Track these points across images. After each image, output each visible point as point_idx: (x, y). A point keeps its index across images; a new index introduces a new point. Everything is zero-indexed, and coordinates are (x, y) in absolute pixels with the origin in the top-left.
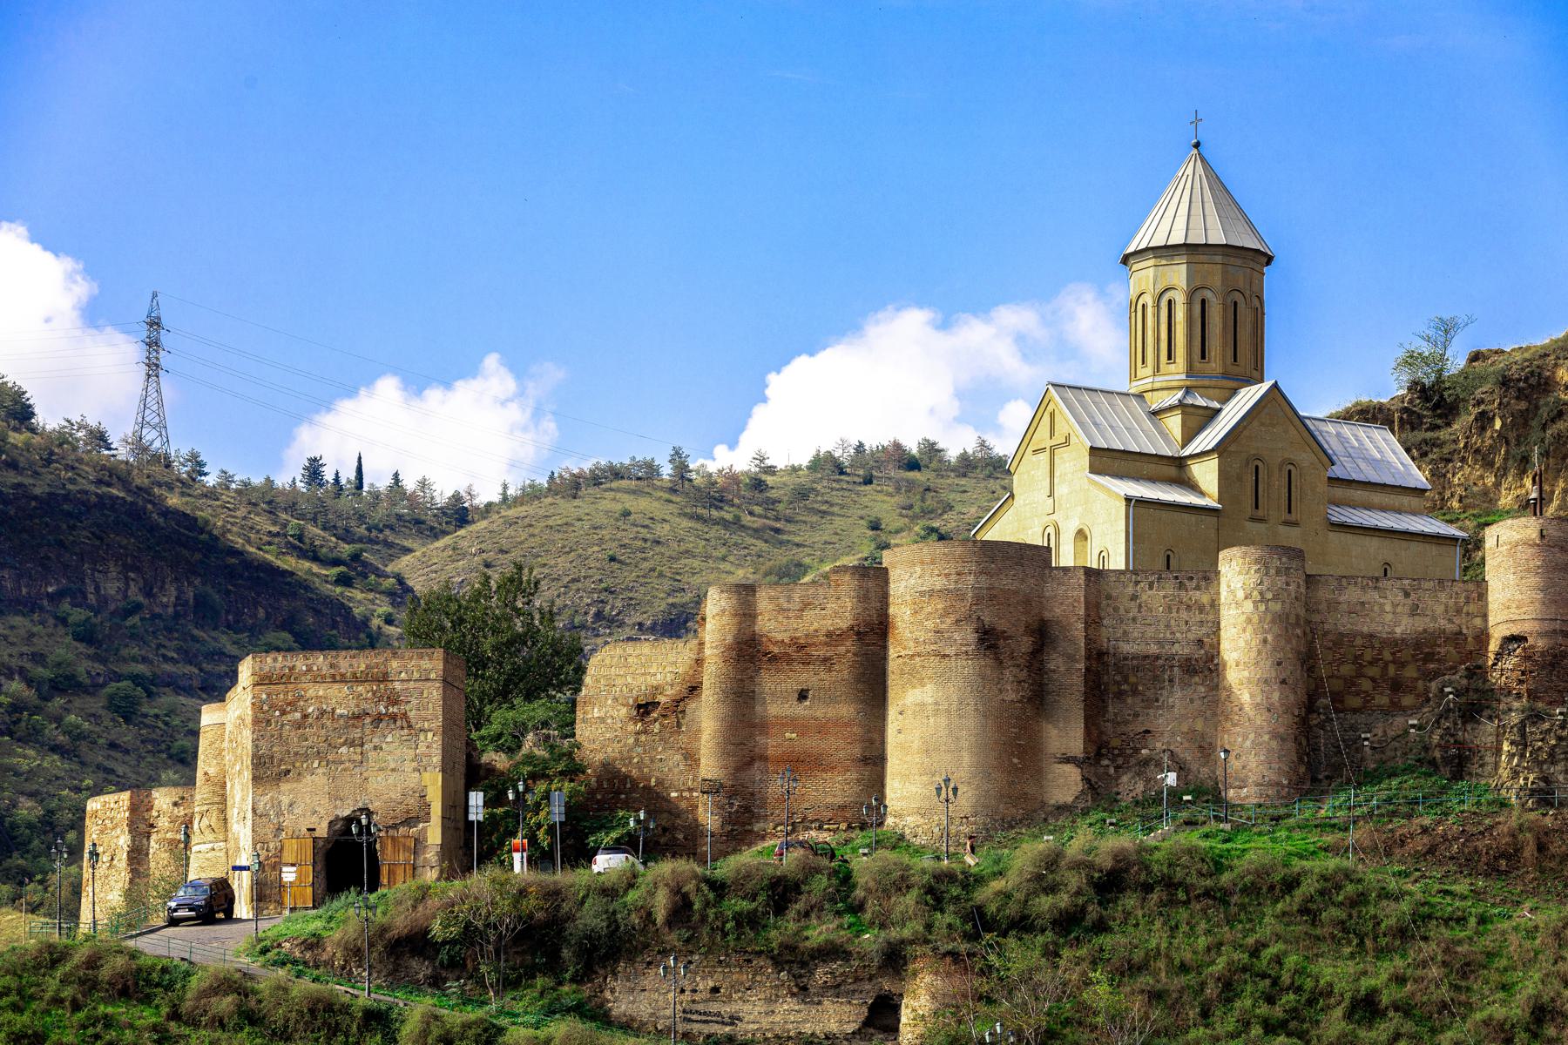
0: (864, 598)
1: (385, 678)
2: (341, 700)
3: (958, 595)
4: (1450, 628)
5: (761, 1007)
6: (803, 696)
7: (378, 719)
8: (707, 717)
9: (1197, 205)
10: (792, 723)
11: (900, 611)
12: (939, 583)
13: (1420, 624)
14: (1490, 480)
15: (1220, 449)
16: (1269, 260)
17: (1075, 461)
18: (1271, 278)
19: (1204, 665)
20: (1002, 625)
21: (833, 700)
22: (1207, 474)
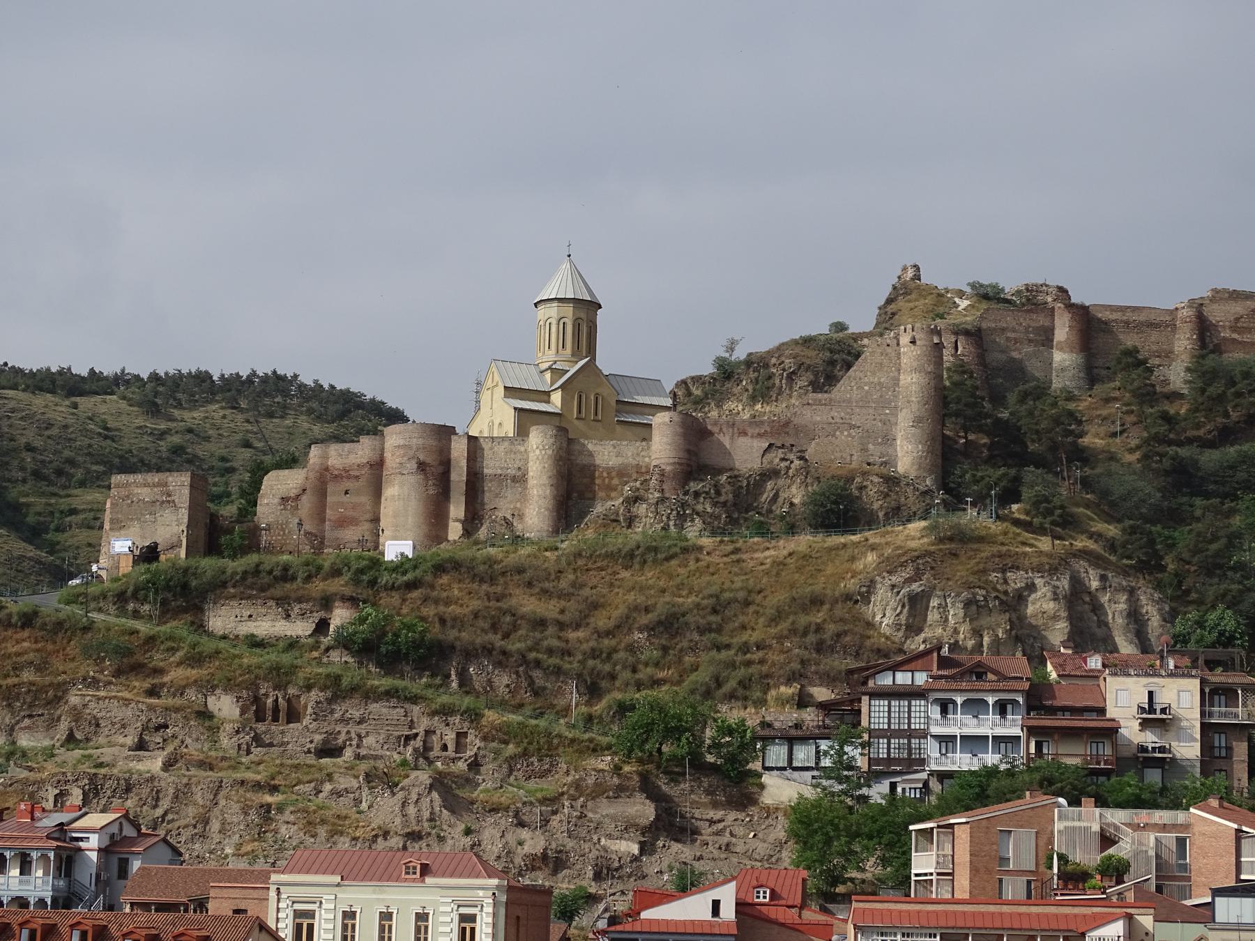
1: (166, 485)
2: (145, 494)
4: (634, 462)
6: (346, 493)
7: (163, 502)
8: (307, 502)
9: (563, 284)
10: (341, 504)
11: (388, 455)
12: (402, 442)
13: (620, 460)
14: (740, 408)
15: (561, 387)
16: (600, 307)
22: (557, 398)
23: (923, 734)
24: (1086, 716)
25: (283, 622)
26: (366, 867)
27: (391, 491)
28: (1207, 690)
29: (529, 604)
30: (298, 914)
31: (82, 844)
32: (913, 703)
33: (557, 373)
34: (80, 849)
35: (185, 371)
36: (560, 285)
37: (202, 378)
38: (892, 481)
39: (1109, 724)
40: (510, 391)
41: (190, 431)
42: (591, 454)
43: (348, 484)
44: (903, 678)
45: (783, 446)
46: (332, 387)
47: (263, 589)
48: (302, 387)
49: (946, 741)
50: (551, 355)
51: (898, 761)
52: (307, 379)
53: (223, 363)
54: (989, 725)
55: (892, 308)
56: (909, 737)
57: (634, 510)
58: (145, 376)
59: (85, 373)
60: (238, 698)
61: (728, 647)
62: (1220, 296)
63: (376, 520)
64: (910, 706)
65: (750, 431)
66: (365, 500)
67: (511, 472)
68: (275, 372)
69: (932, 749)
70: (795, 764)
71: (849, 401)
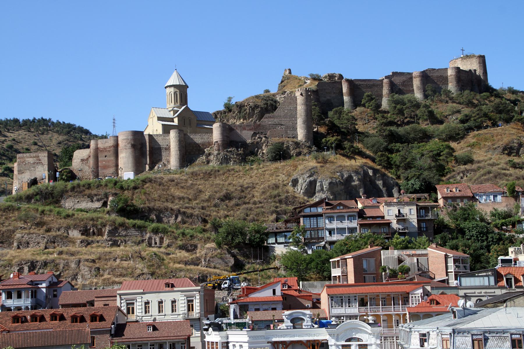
1: (38, 157)
2: (31, 160)
3: (128, 139)
5: (86, 204)
6: (106, 156)
8: (91, 161)
10: (104, 161)
11: (120, 142)
12: (125, 138)
13: (203, 140)
15: (178, 116)
19: (168, 149)
21: (110, 157)
22: (176, 120)
24: (368, 219)
25: (91, 203)
26: (150, 286)
29: (178, 193)
30: (128, 304)
31: (40, 286)
33: (175, 112)
34: (39, 288)
36: (174, 80)
37: (16, 121)
38: (297, 144)
39: (388, 222)
40: (160, 119)
41: (14, 140)
42: (192, 139)
43: (106, 154)
44: (314, 210)
45: (259, 133)
46: (64, 123)
47: (81, 192)
48: (53, 123)
50: (172, 105)
53: (23, 114)
54: (346, 224)
57: (209, 158)
60: (80, 231)
61: (249, 203)
62: (395, 74)
63: (117, 165)
65: (247, 128)
66: (113, 158)
68: (42, 118)
70: (278, 241)
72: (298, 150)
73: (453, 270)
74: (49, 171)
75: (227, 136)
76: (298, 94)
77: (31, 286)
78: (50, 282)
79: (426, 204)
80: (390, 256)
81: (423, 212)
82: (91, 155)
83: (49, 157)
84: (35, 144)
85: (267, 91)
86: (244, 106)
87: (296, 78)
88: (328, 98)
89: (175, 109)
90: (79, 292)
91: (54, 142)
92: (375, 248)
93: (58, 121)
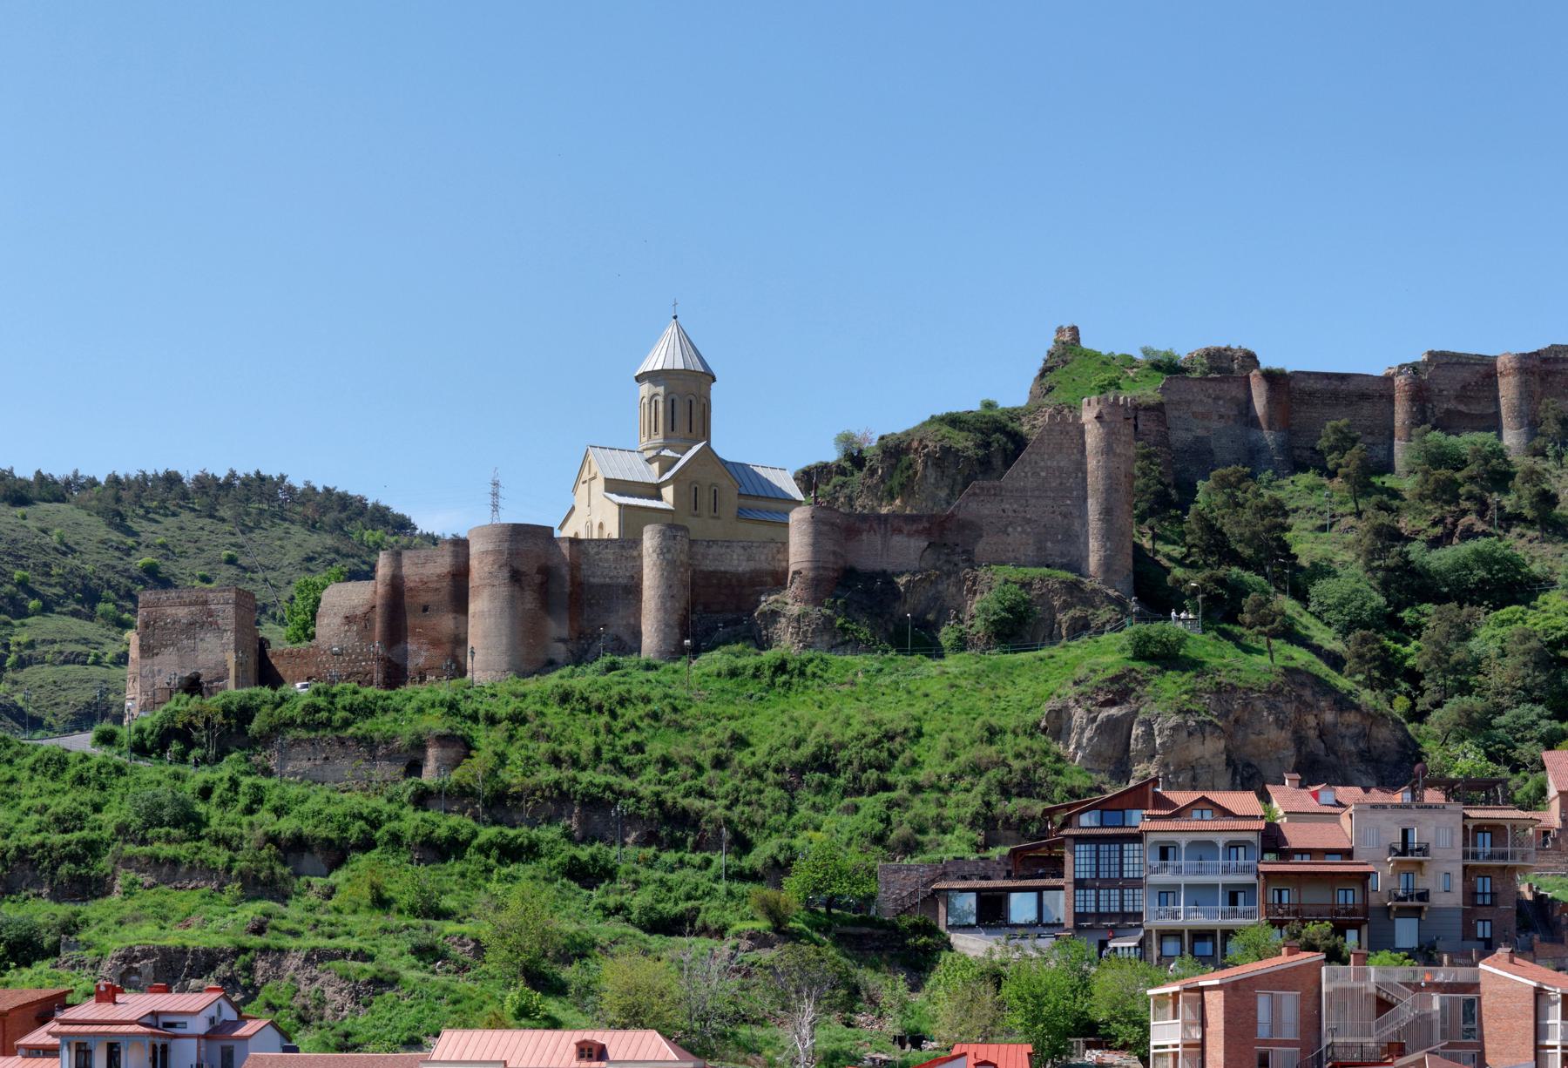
0: (455, 555)
11: (474, 563)
15: (674, 479)
16: (714, 380)
17: (599, 485)
18: (716, 392)
20: (524, 569)
22: (668, 492)
23: (1137, 883)
24: (1297, 858)
26: (530, 1049)
27: (479, 604)
28: (1470, 827)
32: (1126, 846)
33: (667, 464)
35: (150, 472)
36: (663, 355)
37: (172, 479)
40: (613, 486)
48: (291, 490)
49: (1166, 894)
51: (1110, 916)
52: (298, 482)
53: (194, 460)
55: (1051, 379)
56: (1122, 888)
58: (102, 478)
59: (31, 476)
64: (1121, 851)
67: (623, 581)
69: (1145, 904)
71: (1024, 489)
72: (1076, 612)
73: (1557, 1042)
74: (236, 651)
75: (834, 553)
76: (1088, 416)
77: (147, 1030)
78: (212, 1020)
79: (1497, 814)
80: (1348, 985)
81: (1485, 845)
82: (379, 602)
83: (237, 605)
84: (231, 561)
85: (989, 405)
86: (907, 451)
87: (1093, 355)
88: (1200, 432)
89: (667, 453)
90: (304, 1058)
91: (294, 555)
92: (1305, 957)
93: (307, 483)
